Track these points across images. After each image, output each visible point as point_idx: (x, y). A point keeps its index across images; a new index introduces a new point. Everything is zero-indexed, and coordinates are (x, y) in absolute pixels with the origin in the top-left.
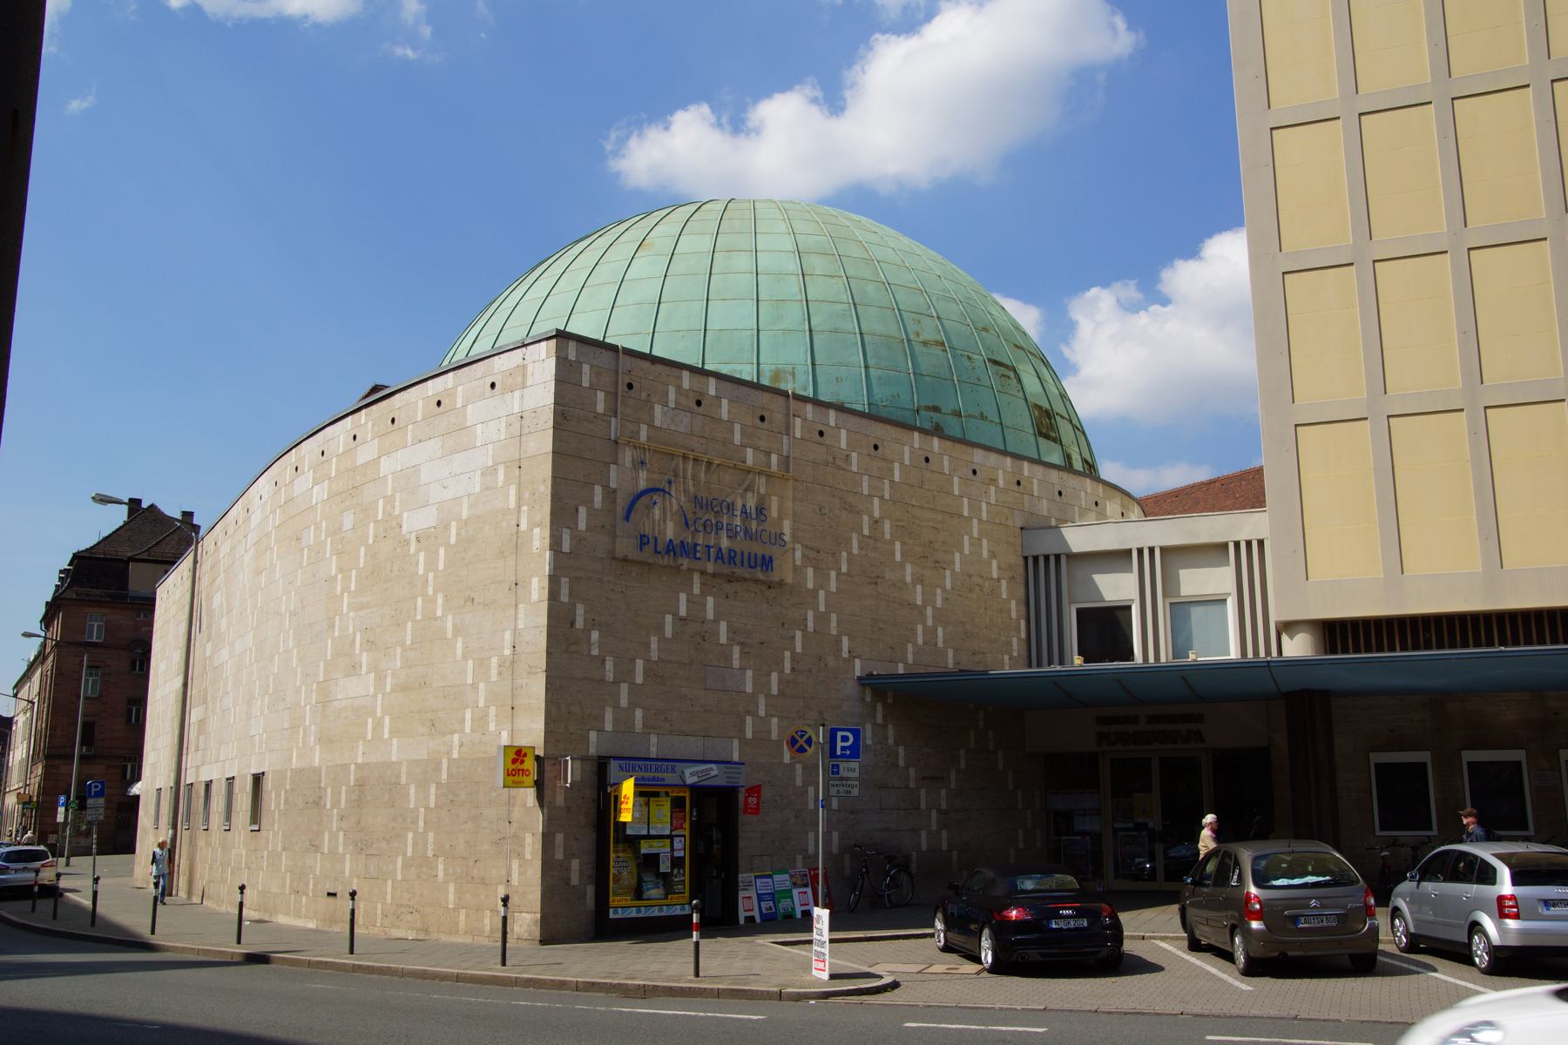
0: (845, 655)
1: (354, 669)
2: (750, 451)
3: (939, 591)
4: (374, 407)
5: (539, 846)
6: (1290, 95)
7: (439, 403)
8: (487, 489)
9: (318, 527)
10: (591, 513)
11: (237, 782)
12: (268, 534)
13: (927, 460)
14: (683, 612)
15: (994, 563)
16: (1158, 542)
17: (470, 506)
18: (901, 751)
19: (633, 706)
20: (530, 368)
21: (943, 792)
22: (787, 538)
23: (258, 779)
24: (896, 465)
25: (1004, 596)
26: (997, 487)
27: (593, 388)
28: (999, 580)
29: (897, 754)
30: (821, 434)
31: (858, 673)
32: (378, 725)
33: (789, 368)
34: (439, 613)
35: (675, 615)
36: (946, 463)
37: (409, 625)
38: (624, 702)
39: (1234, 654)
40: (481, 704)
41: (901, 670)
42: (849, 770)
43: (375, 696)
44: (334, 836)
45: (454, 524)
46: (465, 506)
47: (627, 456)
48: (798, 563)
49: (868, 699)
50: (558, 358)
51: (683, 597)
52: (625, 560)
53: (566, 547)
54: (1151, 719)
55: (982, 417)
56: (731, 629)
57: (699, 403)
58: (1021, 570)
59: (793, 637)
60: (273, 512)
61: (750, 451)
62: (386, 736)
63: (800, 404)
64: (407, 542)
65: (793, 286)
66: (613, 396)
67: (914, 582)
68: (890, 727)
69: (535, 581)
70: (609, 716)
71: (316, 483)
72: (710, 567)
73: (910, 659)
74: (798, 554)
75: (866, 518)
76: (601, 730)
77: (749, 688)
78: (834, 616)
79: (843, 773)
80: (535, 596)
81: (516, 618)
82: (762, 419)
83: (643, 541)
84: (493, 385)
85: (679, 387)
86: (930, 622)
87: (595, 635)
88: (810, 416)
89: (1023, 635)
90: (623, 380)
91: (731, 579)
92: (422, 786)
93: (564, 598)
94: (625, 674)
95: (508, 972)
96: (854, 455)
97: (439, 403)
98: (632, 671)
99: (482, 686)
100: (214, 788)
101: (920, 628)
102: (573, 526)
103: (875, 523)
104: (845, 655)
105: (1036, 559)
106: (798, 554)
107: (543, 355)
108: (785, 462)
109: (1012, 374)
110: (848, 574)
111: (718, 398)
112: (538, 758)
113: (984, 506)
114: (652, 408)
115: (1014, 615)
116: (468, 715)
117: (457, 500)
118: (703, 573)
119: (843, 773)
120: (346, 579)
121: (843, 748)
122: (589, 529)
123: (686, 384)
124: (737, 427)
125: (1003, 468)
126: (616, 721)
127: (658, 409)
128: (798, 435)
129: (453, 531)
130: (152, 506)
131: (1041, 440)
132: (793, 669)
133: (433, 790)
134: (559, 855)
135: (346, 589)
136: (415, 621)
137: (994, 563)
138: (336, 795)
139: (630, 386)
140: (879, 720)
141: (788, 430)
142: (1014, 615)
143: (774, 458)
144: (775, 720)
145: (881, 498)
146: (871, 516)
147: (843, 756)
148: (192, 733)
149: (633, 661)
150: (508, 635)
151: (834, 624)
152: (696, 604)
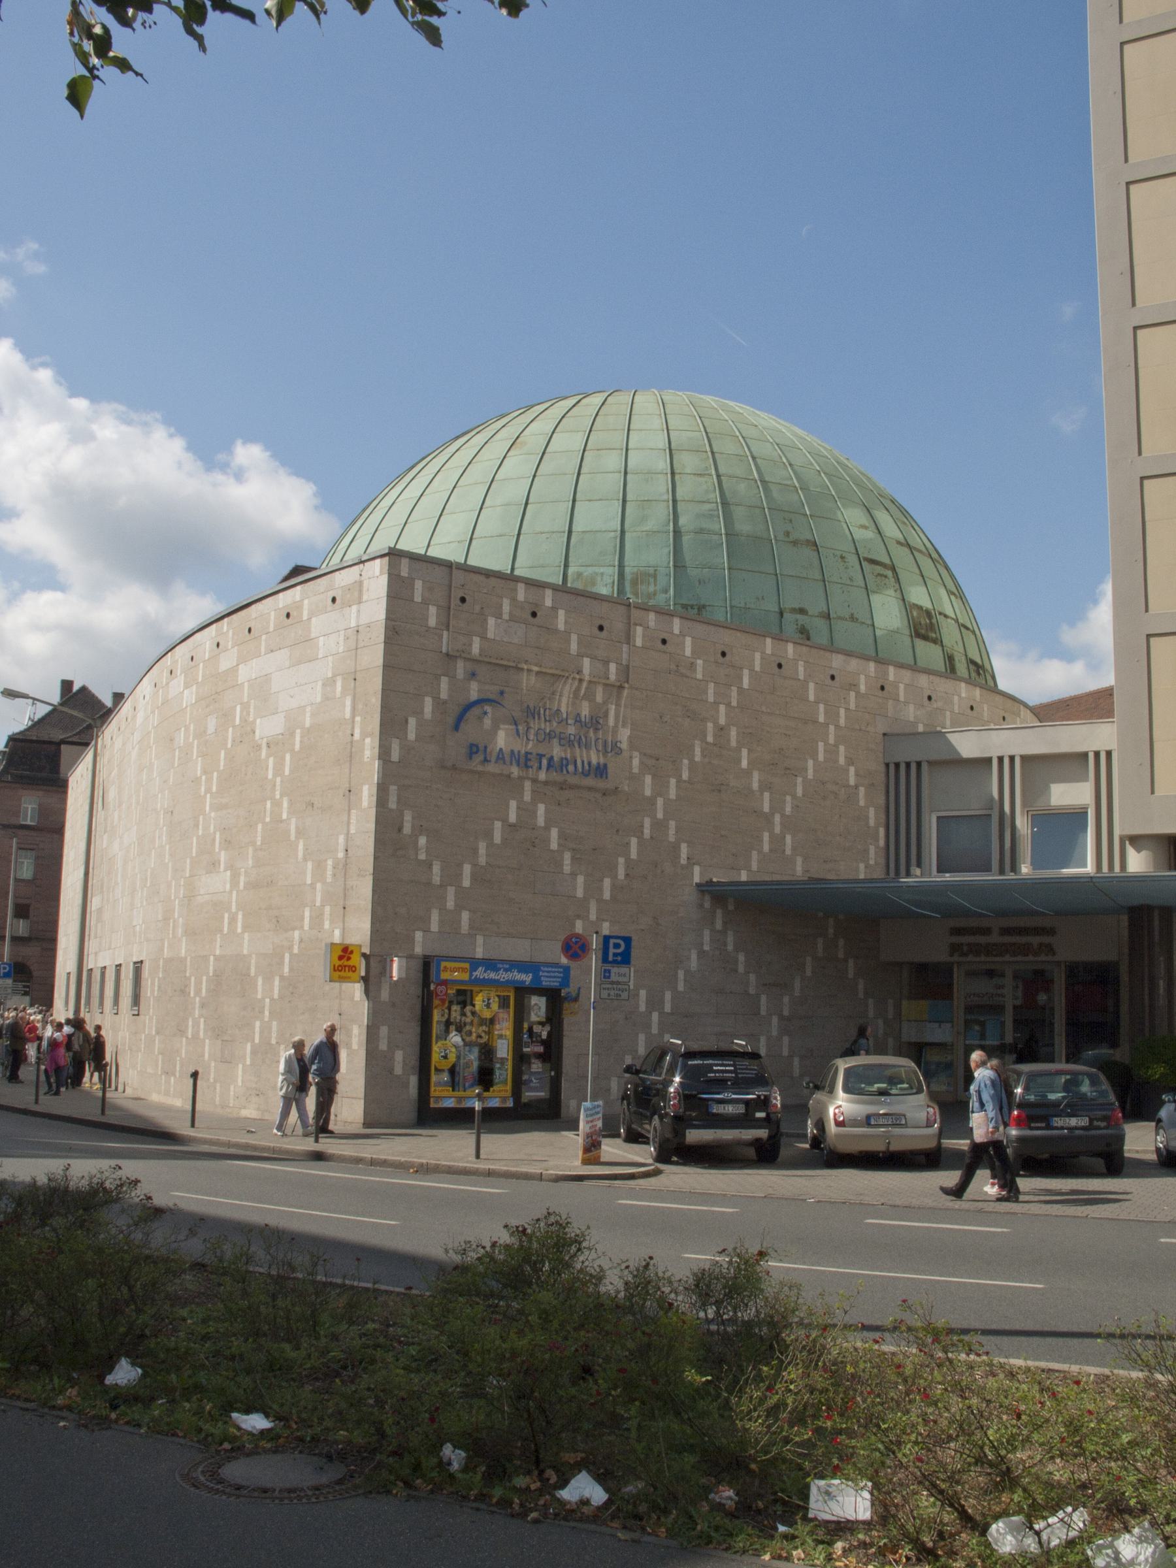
0: (683, 861)
1: (214, 865)
2: (586, 662)
3: (788, 798)
4: (234, 617)
5: (364, 1037)
7: (288, 615)
8: (327, 699)
9: (187, 728)
10: (421, 724)
12: (149, 733)
13: (780, 666)
14: (513, 818)
15: (852, 769)
17: (312, 715)
18: (741, 957)
19: (459, 907)
20: (365, 583)
21: (786, 999)
23: (138, 966)
24: (746, 672)
25: (862, 803)
26: (858, 693)
27: (425, 602)
28: (856, 787)
29: (736, 961)
30: (664, 642)
31: (697, 879)
32: (233, 920)
33: (651, 570)
34: (284, 816)
35: (505, 820)
36: (801, 669)
37: (260, 826)
38: (450, 904)
39: (1089, 868)
40: (318, 904)
41: (744, 877)
42: (620, 975)
43: (231, 892)
44: (196, 1025)
45: (298, 731)
46: (308, 715)
47: (460, 669)
49: (707, 905)
50: (390, 575)
51: (513, 804)
53: (395, 756)
54: (1006, 931)
55: (853, 618)
56: (563, 836)
57: (534, 614)
59: (628, 844)
60: (153, 712)
61: (586, 662)
62: (239, 930)
63: (643, 613)
64: (259, 747)
65: (661, 486)
68: (730, 933)
69: (366, 788)
70: (435, 917)
71: (187, 686)
72: (542, 776)
73: (754, 867)
74: (636, 762)
75: (710, 725)
76: (426, 931)
77: (580, 893)
78: (672, 824)
79: (614, 978)
80: (365, 804)
81: (349, 823)
82: (601, 628)
83: (473, 750)
84: (334, 600)
85: (514, 599)
86: (777, 830)
87: (422, 841)
88: (652, 624)
89: (882, 843)
90: (457, 594)
91: (563, 786)
92: (268, 979)
93: (392, 805)
94: (452, 877)
95: (482, 1166)
96: (700, 662)
97: (288, 615)
99: (319, 886)
100: (107, 971)
101: (766, 836)
102: (403, 736)
103: (721, 730)
104: (683, 861)
106: (636, 762)
107: (377, 572)
108: (625, 671)
109: (889, 573)
110: (690, 782)
111: (554, 609)
112: (364, 955)
113: (842, 711)
114: (486, 620)
115: (872, 823)
116: (307, 914)
117: (302, 709)
118: (535, 781)
121: (615, 955)
122: (419, 738)
123: (521, 596)
124: (574, 637)
125: (865, 673)
126: (442, 922)
127: (491, 621)
129: (298, 739)
130: (84, 689)
131: (919, 643)
132: (627, 875)
133: (277, 983)
135: (208, 790)
136: (264, 823)
137: (852, 769)
138: (199, 983)
139: (463, 600)
140: (719, 925)
141: (629, 638)
142: (872, 823)
143: (613, 667)
145: (728, 705)
146: (716, 723)
147: (615, 962)
148: (92, 920)
150: (341, 839)
151: (672, 831)
152: (527, 812)
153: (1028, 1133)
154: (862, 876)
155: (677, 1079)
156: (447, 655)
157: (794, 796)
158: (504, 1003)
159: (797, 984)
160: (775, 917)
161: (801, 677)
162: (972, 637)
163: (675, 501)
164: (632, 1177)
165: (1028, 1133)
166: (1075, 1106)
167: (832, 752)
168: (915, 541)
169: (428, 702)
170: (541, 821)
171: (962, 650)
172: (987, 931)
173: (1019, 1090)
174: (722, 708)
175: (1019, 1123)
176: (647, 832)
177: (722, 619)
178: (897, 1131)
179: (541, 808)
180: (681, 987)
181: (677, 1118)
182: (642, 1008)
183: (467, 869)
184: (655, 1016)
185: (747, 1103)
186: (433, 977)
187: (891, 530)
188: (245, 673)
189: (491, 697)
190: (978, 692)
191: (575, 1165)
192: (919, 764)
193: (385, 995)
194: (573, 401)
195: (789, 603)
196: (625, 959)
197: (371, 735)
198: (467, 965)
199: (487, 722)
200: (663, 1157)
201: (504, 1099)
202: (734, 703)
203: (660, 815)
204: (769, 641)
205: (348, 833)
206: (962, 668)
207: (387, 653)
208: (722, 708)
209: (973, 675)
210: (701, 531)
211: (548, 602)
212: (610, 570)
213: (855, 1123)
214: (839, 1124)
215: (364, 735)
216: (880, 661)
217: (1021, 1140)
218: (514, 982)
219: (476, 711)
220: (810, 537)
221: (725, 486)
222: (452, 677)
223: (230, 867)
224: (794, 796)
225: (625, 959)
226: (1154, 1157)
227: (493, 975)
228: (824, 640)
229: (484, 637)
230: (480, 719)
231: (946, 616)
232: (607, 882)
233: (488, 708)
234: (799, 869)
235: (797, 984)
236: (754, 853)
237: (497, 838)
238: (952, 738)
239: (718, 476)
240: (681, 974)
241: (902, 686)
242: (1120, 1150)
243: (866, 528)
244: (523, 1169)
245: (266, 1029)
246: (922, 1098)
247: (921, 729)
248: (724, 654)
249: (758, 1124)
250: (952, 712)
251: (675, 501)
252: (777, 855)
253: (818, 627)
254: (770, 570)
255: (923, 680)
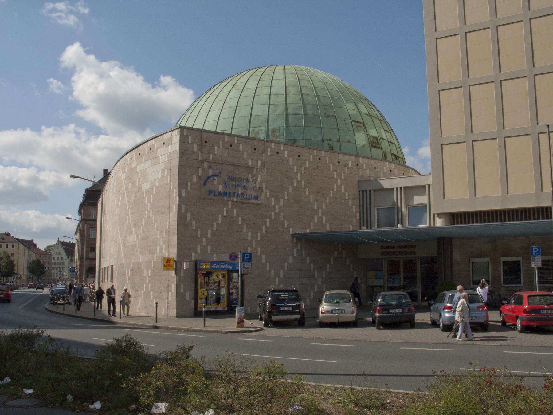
0: (286, 226)
2: (250, 160)
3: (324, 204)
4: (136, 150)
6: (443, 26)
11: (114, 266)
13: (320, 159)
14: (225, 214)
15: (347, 194)
16: (403, 185)
18: (308, 258)
19: (207, 245)
21: (324, 272)
22: (264, 189)
24: (307, 162)
25: (351, 205)
26: (348, 167)
27: (193, 143)
28: (348, 199)
30: (278, 153)
31: (291, 233)
32: (137, 251)
35: (222, 215)
36: (327, 160)
38: (204, 243)
39: (427, 225)
41: (308, 231)
47: (206, 165)
48: (268, 196)
49: (295, 241)
51: (225, 210)
52: (204, 198)
53: (184, 195)
54: (399, 247)
55: (348, 141)
56: (243, 219)
57: (231, 146)
58: (358, 196)
59: (266, 221)
64: (143, 193)
65: (282, 99)
66: (200, 146)
67: (314, 201)
68: (303, 250)
69: (174, 206)
72: (235, 199)
73: (312, 227)
74: (268, 194)
75: (295, 180)
76: (196, 252)
77: (249, 238)
78: (282, 214)
79: (246, 267)
82: (255, 149)
83: (210, 192)
84: (164, 143)
85: (224, 141)
86: (320, 215)
87: (194, 223)
88: (273, 147)
89: (358, 218)
91: (242, 203)
92: (147, 270)
93: (183, 211)
96: (290, 159)
98: (207, 234)
101: (316, 217)
103: (299, 182)
104: (286, 226)
105: (363, 191)
106: (268, 194)
107: (176, 133)
109: (362, 125)
111: (238, 143)
112: (175, 261)
113: (343, 174)
115: (354, 211)
117: (155, 180)
118: (233, 201)
119: (246, 267)
120: (130, 204)
122: (191, 189)
123: (226, 140)
126: (201, 250)
127: (216, 149)
128: (269, 153)
131: (372, 148)
132: (266, 232)
134: (182, 291)
135: (129, 208)
137: (347, 194)
138: (128, 272)
139: (206, 142)
140: (299, 248)
141: (265, 152)
142: (354, 211)
143: (259, 162)
144: (259, 249)
145: (301, 173)
147: (246, 261)
149: (207, 230)
152: (230, 212)
153: (382, 315)
154: (351, 230)
155: (269, 299)
156: (201, 160)
157: (326, 203)
158: (224, 276)
159: (328, 266)
160: (321, 246)
161: (328, 163)
162: (394, 146)
163: (286, 104)
164: (251, 331)
165: (382, 315)
166: (397, 306)
167: (339, 187)
168: (374, 113)
169: (195, 176)
170: (235, 215)
171: (389, 150)
172: (393, 247)
173: (379, 300)
174: (299, 174)
175: (379, 311)
176: (273, 217)
177: (302, 145)
178: (341, 315)
179: (235, 211)
180: (286, 269)
181: (269, 312)
182: (273, 276)
183: (210, 232)
184: (277, 279)
185: (292, 306)
186: (198, 268)
187: (363, 109)
188: (139, 169)
189: (216, 174)
190: (393, 165)
191: (234, 328)
192: (370, 191)
193: (182, 274)
194: (255, 70)
195: (326, 137)
196: (250, 260)
197: (175, 188)
198: (209, 263)
199: (215, 183)
200: (266, 325)
201: (224, 308)
202: (303, 173)
203: (277, 211)
204: (315, 151)
205: (169, 221)
206: (389, 157)
207: (180, 161)
208: (299, 174)
209: (394, 159)
210: (295, 114)
211: (236, 141)
212: (264, 129)
213: (328, 312)
214: (322, 313)
215: (174, 188)
216: (357, 156)
217: (379, 317)
218: (226, 269)
219: (211, 179)
220: (333, 114)
221: (304, 97)
222: (203, 168)
223: (136, 233)
224: (326, 203)
225: (250, 260)
226: (430, 322)
227: (218, 267)
228: (338, 150)
229: (213, 154)
230: (213, 181)
231: (383, 139)
232: (259, 234)
233: (216, 178)
234: (328, 228)
235: (328, 266)
236: (312, 223)
237: (220, 221)
238: (381, 182)
239: (302, 95)
240: (286, 264)
241: (364, 164)
242: (414, 320)
243: (354, 110)
244: (217, 330)
245: (147, 287)
246: (351, 304)
247: (372, 178)
248: (299, 156)
249: (296, 314)
250: (383, 172)
251: (286, 104)
252: (320, 223)
253: (336, 145)
254: (319, 125)
255: (372, 162)
